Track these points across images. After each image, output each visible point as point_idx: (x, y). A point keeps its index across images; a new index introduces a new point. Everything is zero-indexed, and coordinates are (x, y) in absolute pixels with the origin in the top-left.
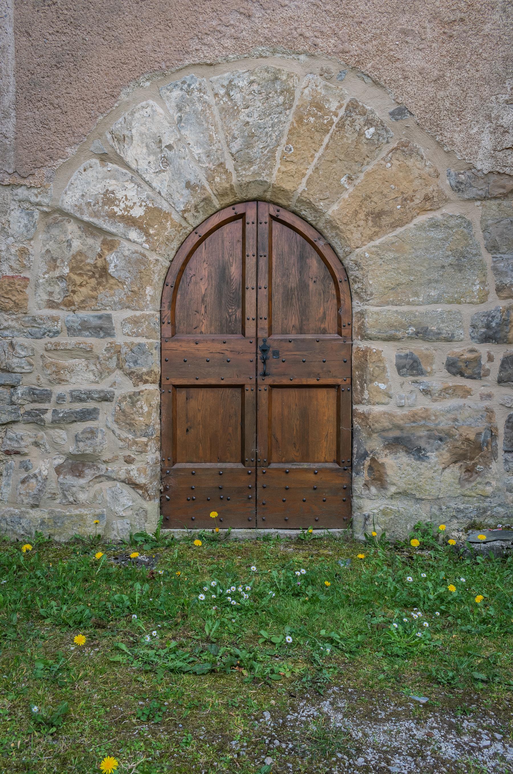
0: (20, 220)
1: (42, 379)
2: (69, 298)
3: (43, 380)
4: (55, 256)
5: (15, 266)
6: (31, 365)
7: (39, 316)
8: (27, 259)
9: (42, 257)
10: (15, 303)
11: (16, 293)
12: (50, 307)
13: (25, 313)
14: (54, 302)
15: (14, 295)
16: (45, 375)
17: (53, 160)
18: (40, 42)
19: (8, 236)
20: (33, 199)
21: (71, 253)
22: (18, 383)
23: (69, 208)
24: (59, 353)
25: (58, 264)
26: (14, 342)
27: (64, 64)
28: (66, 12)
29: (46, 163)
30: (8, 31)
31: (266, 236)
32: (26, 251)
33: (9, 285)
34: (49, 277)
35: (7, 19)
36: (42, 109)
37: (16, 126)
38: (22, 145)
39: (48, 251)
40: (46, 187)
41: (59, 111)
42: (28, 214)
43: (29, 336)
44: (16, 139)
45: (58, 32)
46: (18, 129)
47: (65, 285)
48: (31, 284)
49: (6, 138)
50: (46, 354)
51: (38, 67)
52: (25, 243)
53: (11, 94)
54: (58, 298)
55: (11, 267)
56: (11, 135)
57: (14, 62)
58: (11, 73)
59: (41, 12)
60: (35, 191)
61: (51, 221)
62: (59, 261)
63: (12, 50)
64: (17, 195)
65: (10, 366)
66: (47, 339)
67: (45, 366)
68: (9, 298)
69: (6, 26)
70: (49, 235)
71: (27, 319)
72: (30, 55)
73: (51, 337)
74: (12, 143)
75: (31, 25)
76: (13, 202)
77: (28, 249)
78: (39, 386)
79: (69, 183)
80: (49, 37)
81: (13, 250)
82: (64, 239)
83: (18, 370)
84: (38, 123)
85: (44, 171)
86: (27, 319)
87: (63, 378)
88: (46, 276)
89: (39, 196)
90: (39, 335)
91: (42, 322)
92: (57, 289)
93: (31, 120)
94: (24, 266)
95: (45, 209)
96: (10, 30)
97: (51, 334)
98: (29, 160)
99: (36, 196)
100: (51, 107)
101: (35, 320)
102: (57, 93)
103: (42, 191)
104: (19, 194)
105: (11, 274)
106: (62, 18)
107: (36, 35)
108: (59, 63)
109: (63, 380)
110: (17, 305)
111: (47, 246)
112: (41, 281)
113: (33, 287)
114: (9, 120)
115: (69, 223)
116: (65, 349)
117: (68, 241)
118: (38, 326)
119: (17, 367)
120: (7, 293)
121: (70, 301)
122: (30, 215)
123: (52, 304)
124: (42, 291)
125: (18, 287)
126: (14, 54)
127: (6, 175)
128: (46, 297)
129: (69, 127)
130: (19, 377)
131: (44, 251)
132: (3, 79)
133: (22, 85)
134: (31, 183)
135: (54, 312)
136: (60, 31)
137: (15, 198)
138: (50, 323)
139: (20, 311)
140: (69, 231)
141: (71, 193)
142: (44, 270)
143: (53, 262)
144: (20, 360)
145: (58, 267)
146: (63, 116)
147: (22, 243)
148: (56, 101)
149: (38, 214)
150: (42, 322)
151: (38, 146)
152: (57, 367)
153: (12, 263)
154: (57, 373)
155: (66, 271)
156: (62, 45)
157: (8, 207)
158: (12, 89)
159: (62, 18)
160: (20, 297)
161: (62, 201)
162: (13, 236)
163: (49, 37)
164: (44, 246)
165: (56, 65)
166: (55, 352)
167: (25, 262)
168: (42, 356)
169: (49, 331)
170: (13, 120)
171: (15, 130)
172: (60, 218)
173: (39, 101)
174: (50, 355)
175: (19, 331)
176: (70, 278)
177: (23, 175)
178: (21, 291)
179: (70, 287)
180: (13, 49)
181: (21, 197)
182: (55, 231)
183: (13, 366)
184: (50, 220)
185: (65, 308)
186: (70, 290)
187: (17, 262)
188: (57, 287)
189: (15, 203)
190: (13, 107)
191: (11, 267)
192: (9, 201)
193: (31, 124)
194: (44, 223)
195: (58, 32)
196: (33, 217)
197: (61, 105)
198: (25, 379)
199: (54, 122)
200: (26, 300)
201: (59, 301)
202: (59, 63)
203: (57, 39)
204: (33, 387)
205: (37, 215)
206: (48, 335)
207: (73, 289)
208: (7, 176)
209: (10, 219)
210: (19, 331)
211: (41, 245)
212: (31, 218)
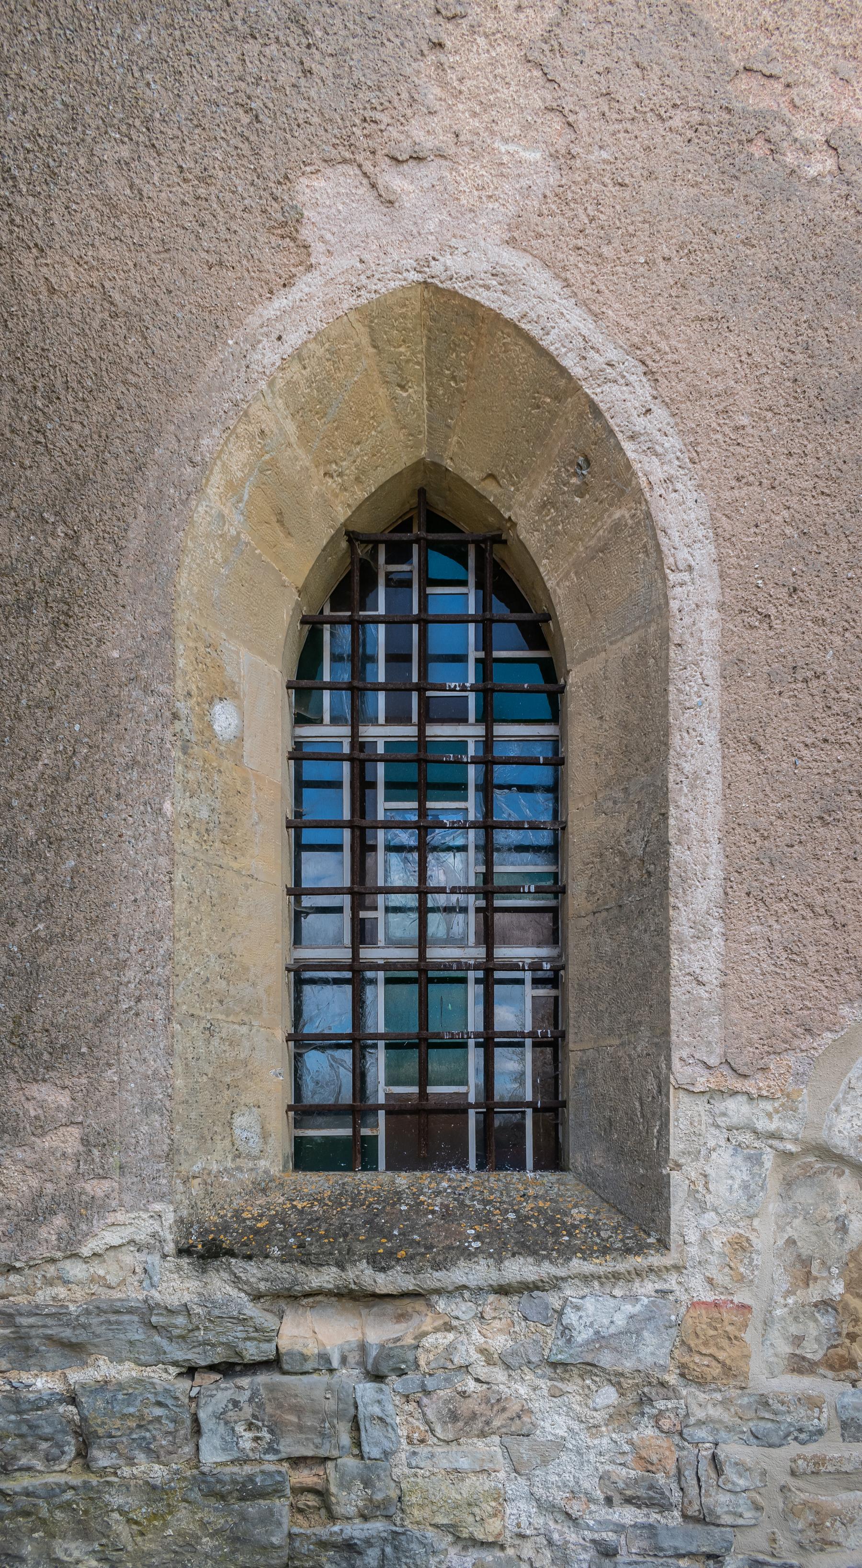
0: (733, 1172)
1: (781, 1541)
2: (840, 1351)
3: (784, 1543)
4: (805, 1252)
5: (721, 1279)
6: (758, 1508)
7: (776, 1395)
8: (746, 1261)
9: (779, 1256)
10: (724, 1365)
11: (725, 1343)
12: (793, 1371)
13: (742, 1388)
14: (804, 1358)
15: (722, 1348)
16: (791, 1531)
17: (811, 1035)
18: (784, 765)
19: (704, 1210)
20: (762, 1124)
21: (847, 1247)
22: (728, 1549)
23: (846, 1144)
24: (821, 1479)
25: (814, 1273)
26: (722, 1457)
27: (840, 815)
28: (846, 696)
29: (796, 1042)
30: (706, 739)
31: (393, 868)
32: (745, 1244)
33: (710, 1325)
34: (796, 1303)
35: (704, 712)
36: (786, 918)
37: (724, 958)
38: (739, 1000)
39: (791, 1242)
40: (794, 1097)
41: (827, 921)
42: (749, 1158)
43: (753, 1440)
44: (723, 985)
45: (826, 741)
46: (729, 966)
47: (832, 1321)
48: (756, 1319)
49: (701, 983)
50: (792, 1482)
51: (779, 822)
52: (741, 1224)
53: (713, 883)
54: (813, 1351)
55: (710, 1281)
56: (712, 977)
57: (719, 811)
58: (713, 836)
59: (786, 695)
60: (768, 1106)
61: (797, 1171)
62: (816, 1264)
63: (715, 782)
64: (724, 1114)
65: (711, 1512)
66: (793, 1449)
67: (790, 1513)
68: (711, 1355)
69: (699, 728)
70: (790, 1204)
71: (746, 1400)
72: (761, 795)
73: (803, 1443)
74: (714, 995)
75: (764, 725)
76: (713, 1130)
77: (748, 1240)
78: (773, 1555)
79: (843, 1086)
80: (805, 752)
81: (717, 1244)
82: (829, 1215)
83: (727, 1519)
84: (778, 950)
85: (790, 1059)
86: (746, 1400)
87: (832, 1537)
88: (790, 1301)
89: (776, 1117)
90: (775, 1440)
91: (784, 1408)
92: (812, 1330)
93: (762, 943)
94: (741, 1279)
95: (791, 1147)
96: (711, 737)
97: (803, 1436)
98: (755, 1036)
99: (769, 1116)
100: (808, 914)
101: (767, 1404)
102: (821, 882)
103: (783, 1105)
104: (730, 1113)
105: (708, 1296)
106: (836, 709)
107: (774, 748)
108: (829, 812)
109: (831, 1543)
110: (727, 1370)
111: (788, 1228)
112: (778, 1312)
113: (760, 1326)
114: (707, 942)
115: (840, 1176)
116: (838, 1472)
117: (837, 1218)
118: (771, 1417)
119: (728, 1513)
120: (706, 1344)
121: (842, 1357)
122: (755, 1160)
123: (800, 1365)
124: (777, 1334)
125: (729, 1328)
126: (720, 792)
127: (699, 1069)
128: (786, 1349)
129: (850, 958)
130: (729, 1537)
131: (781, 1243)
132: (694, 849)
133: (741, 862)
134: (760, 1089)
135: (805, 1384)
136: (832, 739)
137: (720, 1121)
138: (803, 1412)
139: (733, 1383)
140: (842, 1196)
141: (848, 1109)
142: (785, 1287)
143: (804, 1271)
144: (733, 1497)
145: (816, 1279)
146: (836, 933)
147: (735, 1224)
148: (819, 900)
149: (771, 1157)
150: (784, 1408)
151: (776, 1002)
152: (818, 1513)
153: (713, 1272)
154: (817, 1526)
155: (838, 1289)
156: (834, 772)
157: (702, 1141)
158: (715, 871)
159: (836, 709)
160: (735, 1352)
161: (830, 1128)
162: (715, 1210)
163: (805, 752)
164: (781, 1229)
165: (821, 818)
166: (813, 1479)
167: (742, 1270)
168: (783, 1489)
169: (801, 1430)
170: (718, 943)
171: (722, 967)
172: (818, 1166)
173: (781, 899)
174: (800, 1483)
175: (729, 1429)
176: (846, 1307)
177: (743, 1070)
178: (736, 1338)
179: (844, 1326)
180: (718, 780)
181: (735, 1120)
182: (804, 1195)
183: (719, 1511)
184: (794, 1169)
185: (830, 1374)
186: (844, 1332)
187: (727, 1269)
188: (812, 1324)
189: (716, 1132)
190: (716, 912)
191: (710, 1281)
192: (703, 1127)
193: (762, 952)
194: (781, 1177)
195: (826, 741)
196: (761, 1164)
197: (833, 907)
198: (741, 1540)
199: (815, 949)
200: (747, 1357)
201: (817, 1357)
202: (829, 812)
203: (824, 757)
204: (761, 1557)
205: (769, 1159)
206: (796, 1439)
207: (851, 1330)
208: (706, 1072)
209: (709, 1171)
210: (729, 1429)
211: (774, 1227)
212: (756, 1169)
